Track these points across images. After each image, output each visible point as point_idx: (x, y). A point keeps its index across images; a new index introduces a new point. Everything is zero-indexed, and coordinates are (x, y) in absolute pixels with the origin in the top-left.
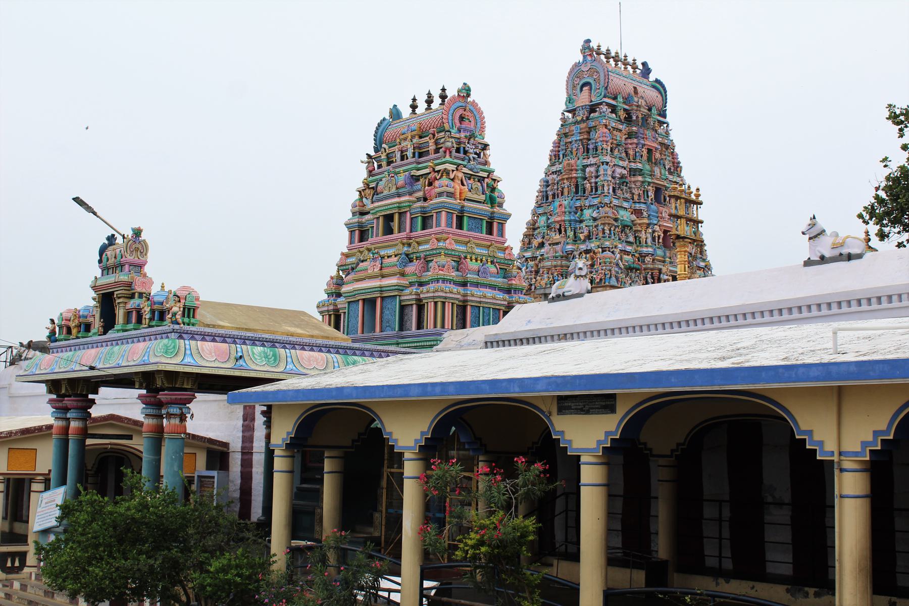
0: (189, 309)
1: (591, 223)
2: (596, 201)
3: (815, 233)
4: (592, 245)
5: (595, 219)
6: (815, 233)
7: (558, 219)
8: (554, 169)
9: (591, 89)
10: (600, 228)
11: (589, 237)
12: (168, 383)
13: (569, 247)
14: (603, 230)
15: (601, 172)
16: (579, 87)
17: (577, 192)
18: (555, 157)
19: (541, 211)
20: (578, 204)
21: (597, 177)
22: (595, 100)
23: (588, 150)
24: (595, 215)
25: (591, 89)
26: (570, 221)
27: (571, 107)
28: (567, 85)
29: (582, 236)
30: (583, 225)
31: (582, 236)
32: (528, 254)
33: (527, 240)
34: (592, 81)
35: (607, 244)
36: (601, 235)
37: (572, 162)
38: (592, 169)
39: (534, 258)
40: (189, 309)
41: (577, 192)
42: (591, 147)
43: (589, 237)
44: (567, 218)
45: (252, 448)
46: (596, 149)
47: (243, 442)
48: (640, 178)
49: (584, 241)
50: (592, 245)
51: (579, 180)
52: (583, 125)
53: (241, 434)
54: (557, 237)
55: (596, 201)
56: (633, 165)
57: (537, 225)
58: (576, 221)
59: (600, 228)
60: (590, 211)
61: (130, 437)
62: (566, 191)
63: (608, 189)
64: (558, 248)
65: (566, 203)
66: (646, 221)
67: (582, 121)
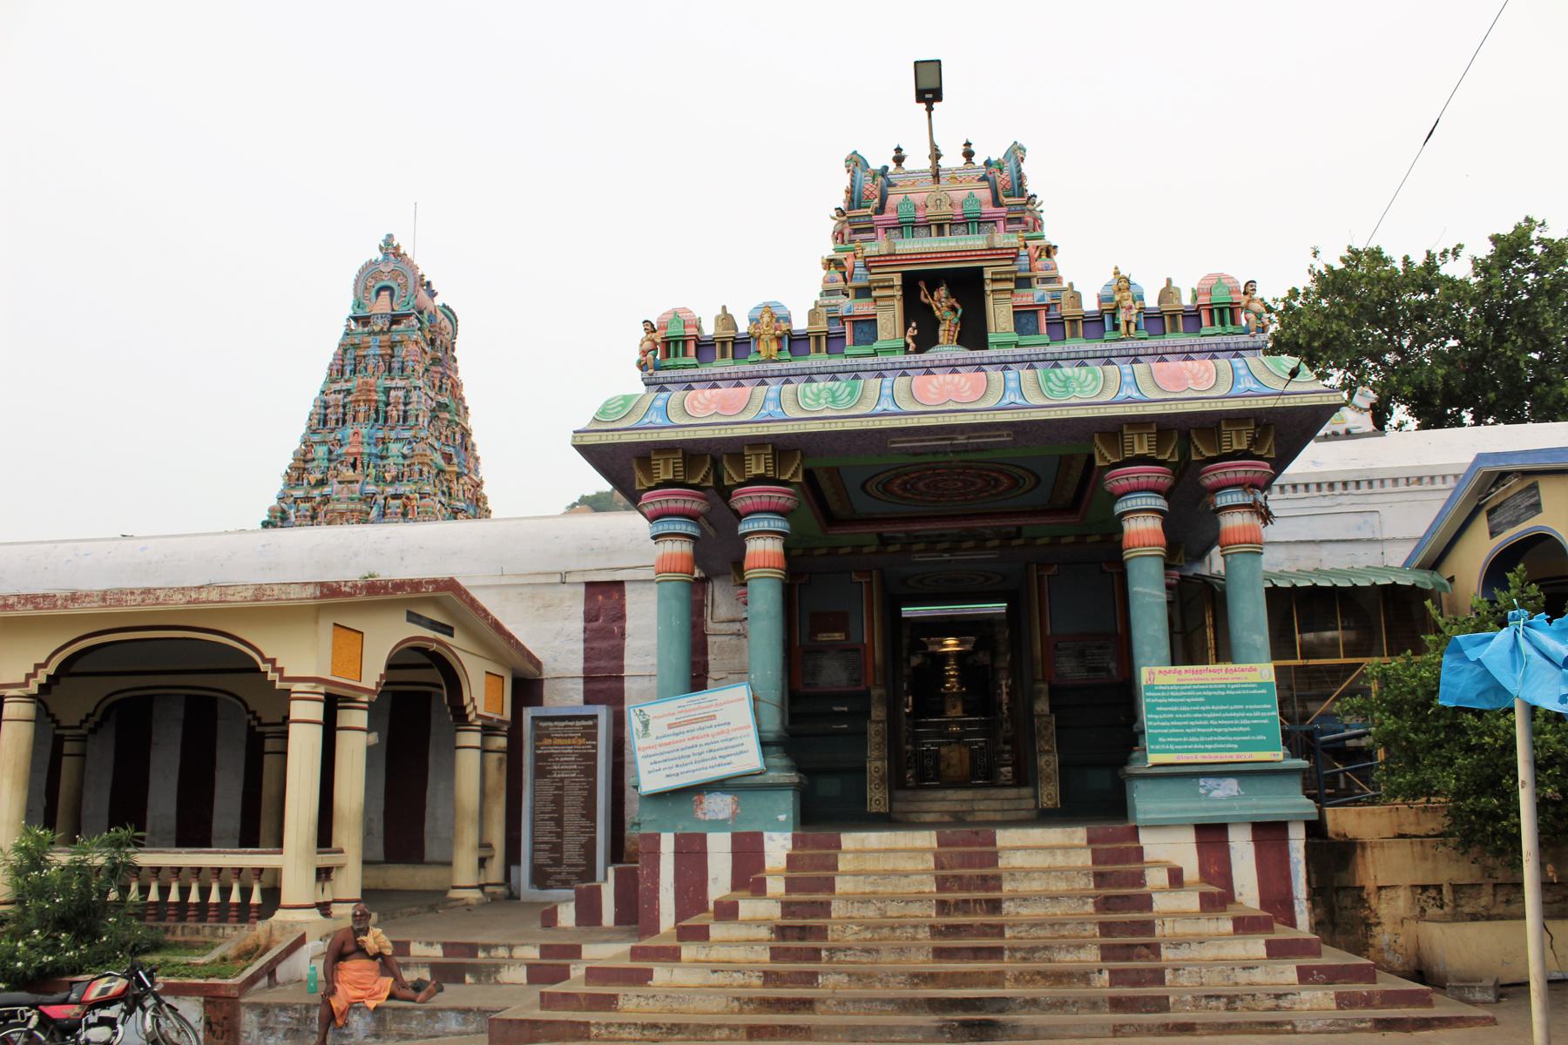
0: (1221, 311)
1: (400, 460)
2: (408, 434)
4: (405, 488)
5: (405, 457)
7: (354, 450)
8: (337, 387)
9: (392, 296)
10: (416, 468)
11: (397, 479)
12: (1208, 450)
13: (371, 488)
14: (421, 472)
15: (414, 399)
16: (373, 291)
17: (376, 420)
18: (337, 372)
19: (317, 438)
20: (380, 434)
21: (406, 404)
22: (400, 310)
23: (390, 370)
24: (406, 451)
25: (392, 296)
26: (370, 455)
27: (361, 313)
28: (357, 282)
29: (388, 477)
30: (390, 461)
31: (388, 477)
32: (299, 493)
33: (295, 474)
34: (394, 285)
35: (427, 489)
36: (417, 476)
37: (372, 381)
38: (401, 393)
39: (308, 499)
40: (1221, 311)
41: (376, 420)
42: (396, 365)
43: (397, 479)
44: (366, 449)
45: (622, 668)
46: (403, 370)
47: (586, 659)
48: (447, 416)
49: (392, 482)
50: (405, 488)
51: (381, 405)
52: (386, 337)
53: (581, 646)
54: (349, 473)
55: (408, 434)
56: (441, 399)
57: (309, 456)
58: (377, 456)
59: (416, 468)
60: (399, 445)
61: (448, 630)
62: (361, 416)
63: (424, 420)
64: (357, 487)
65: (364, 431)
66: (456, 469)
67: (381, 331)
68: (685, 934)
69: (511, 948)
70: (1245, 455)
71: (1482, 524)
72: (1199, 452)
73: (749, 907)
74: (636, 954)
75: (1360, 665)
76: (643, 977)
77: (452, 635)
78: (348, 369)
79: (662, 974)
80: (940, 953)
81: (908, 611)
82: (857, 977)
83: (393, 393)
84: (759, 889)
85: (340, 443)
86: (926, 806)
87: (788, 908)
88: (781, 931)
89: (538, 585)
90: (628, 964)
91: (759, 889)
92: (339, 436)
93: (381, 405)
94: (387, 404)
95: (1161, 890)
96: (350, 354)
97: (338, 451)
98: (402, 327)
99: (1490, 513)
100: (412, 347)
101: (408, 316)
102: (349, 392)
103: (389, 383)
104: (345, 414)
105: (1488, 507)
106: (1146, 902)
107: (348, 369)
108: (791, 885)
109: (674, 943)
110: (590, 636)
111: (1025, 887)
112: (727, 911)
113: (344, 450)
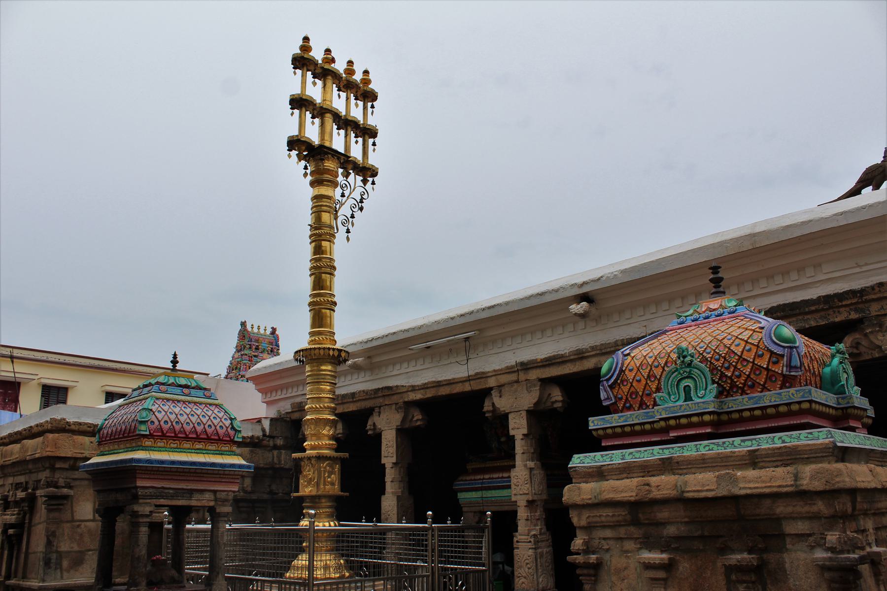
3: (306, 47)
6: (306, 47)
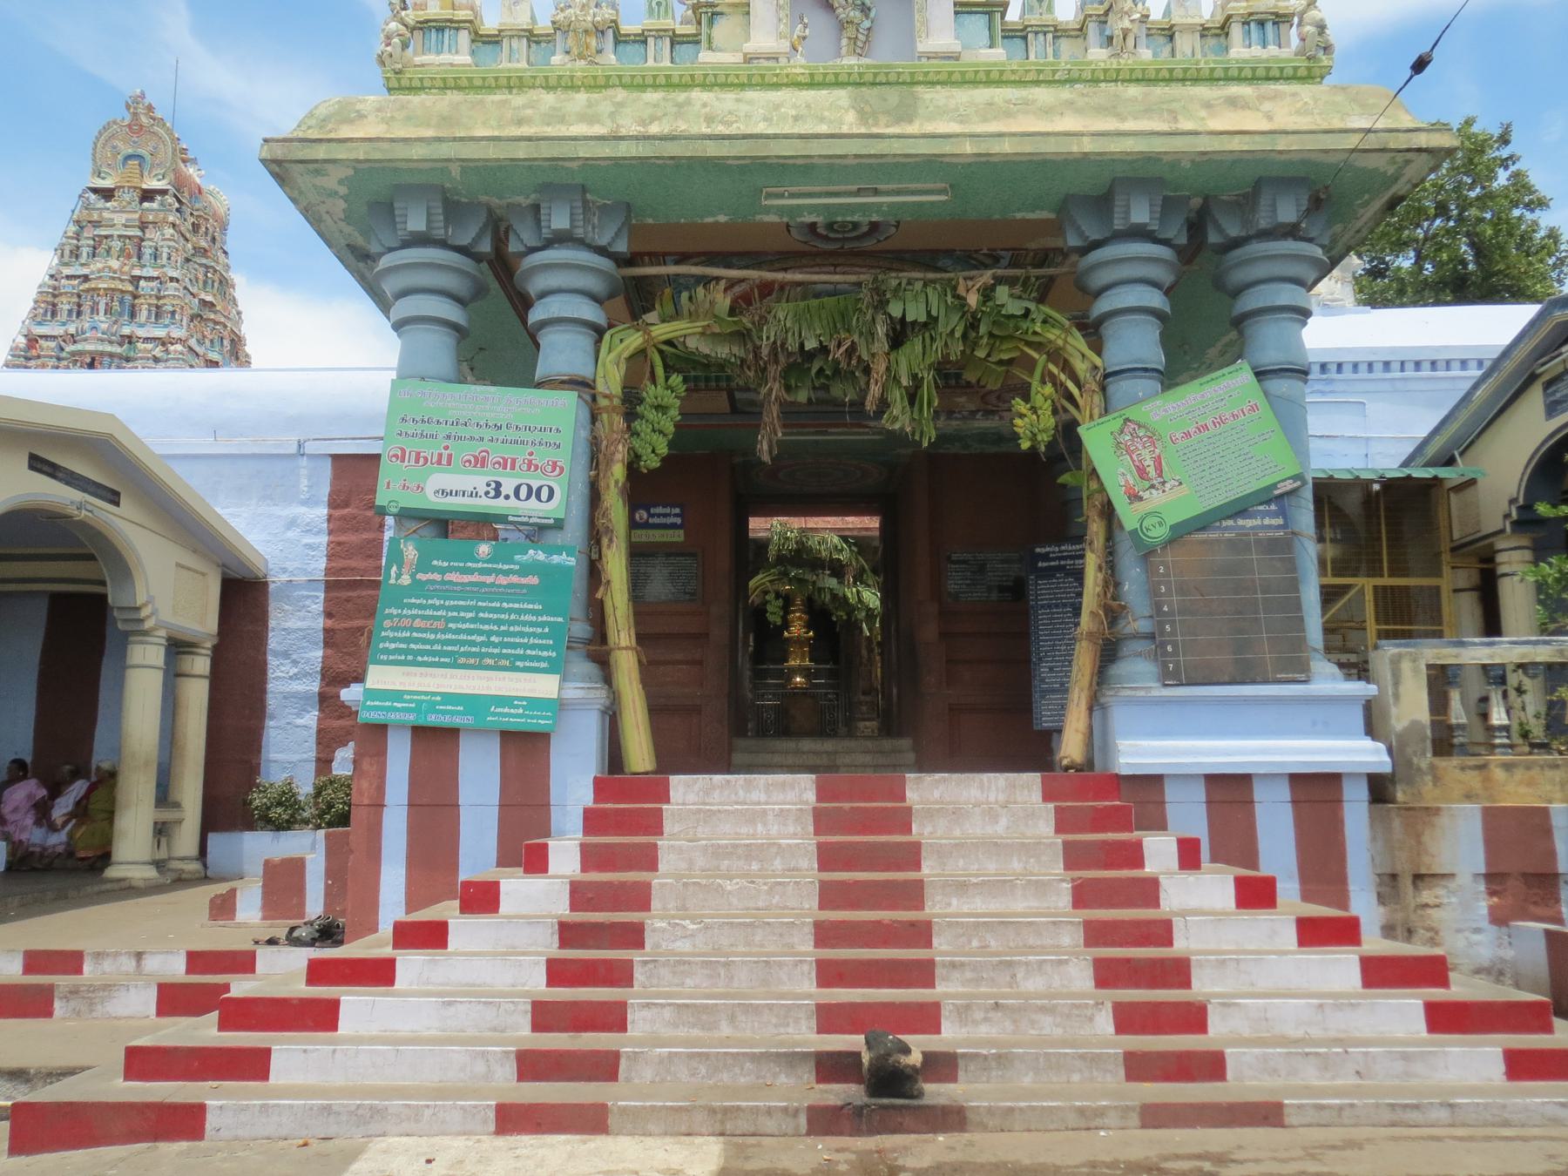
20: (126, 331)
42: (147, 252)
61: (113, 497)
62: (102, 307)
68: (408, 936)
69: (139, 956)
70: (1291, 232)
71: (1535, 398)
72: (1220, 230)
73: (517, 889)
74: (318, 972)
75: (1347, 588)
76: (323, 1017)
77: (117, 504)
78: (85, 251)
79: (355, 1004)
80: (1154, 1116)
81: (758, 526)
82: (700, 1014)
83: (142, 283)
84: (536, 862)
85: (73, 339)
86: (1260, 271)
87: (580, 895)
88: (569, 933)
89: (264, 468)
90: (301, 989)
91: (536, 862)
92: (72, 330)
93: (128, 298)
94: (135, 297)
95: (1170, 873)
96: (89, 232)
97: (70, 348)
98: (155, 205)
99: (1548, 385)
100: (169, 231)
101: (163, 192)
102: (86, 278)
103: (137, 272)
104: (79, 305)
105: (1546, 378)
106: (1149, 891)
107: (85, 251)
108: (590, 858)
109: (387, 951)
110: (336, 525)
111: (959, 866)
112: (482, 899)
113: (79, 347)
